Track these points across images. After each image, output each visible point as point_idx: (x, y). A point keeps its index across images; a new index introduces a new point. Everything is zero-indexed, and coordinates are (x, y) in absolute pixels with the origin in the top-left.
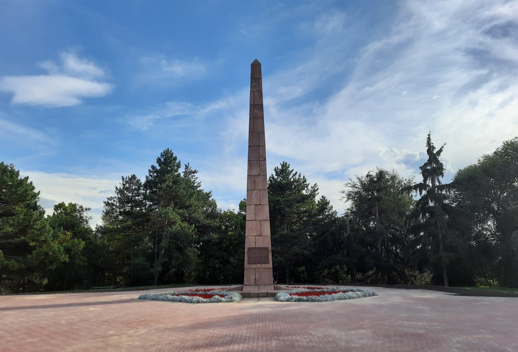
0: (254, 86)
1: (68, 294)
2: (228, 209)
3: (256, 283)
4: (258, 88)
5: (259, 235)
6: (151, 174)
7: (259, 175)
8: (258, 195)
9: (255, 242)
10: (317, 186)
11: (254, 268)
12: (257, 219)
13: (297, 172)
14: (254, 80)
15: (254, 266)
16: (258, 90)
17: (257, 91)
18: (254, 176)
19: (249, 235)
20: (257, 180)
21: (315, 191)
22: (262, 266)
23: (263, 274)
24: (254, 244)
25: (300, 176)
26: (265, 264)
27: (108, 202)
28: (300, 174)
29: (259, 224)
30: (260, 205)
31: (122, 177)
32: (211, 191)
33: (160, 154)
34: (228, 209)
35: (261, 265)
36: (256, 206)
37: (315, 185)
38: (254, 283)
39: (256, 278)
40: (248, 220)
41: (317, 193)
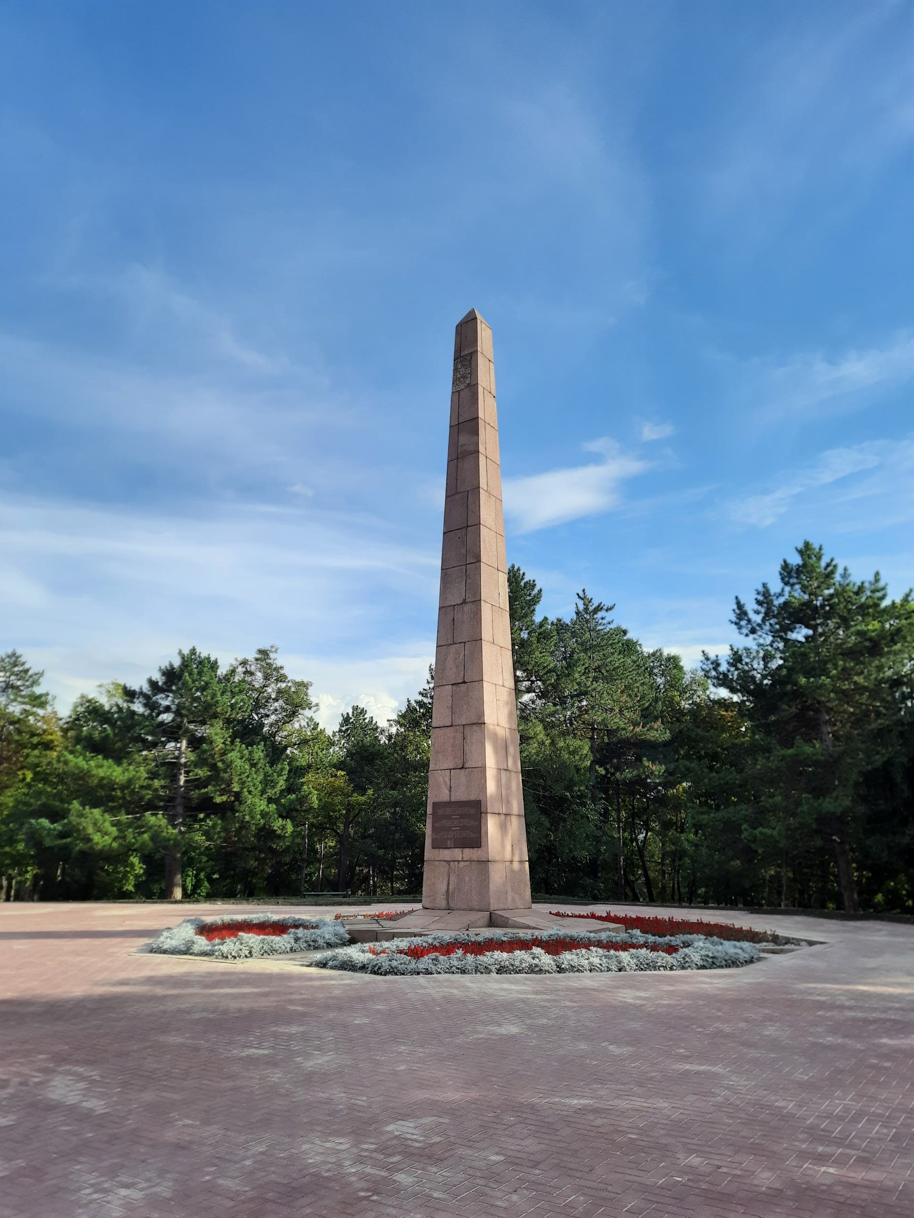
0: (459, 378)
5: (460, 766)
7: (464, 602)
11: (446, 859)
14: (461, 362)
15: (446, 854)
20: (458, 616)
23: (467, 878)
24: (448, 792)
28: (845, 569)
29: (459, 736)
30: (464, 682)
35: (462, 852)
36: (454, 687)
38: (443, 904)
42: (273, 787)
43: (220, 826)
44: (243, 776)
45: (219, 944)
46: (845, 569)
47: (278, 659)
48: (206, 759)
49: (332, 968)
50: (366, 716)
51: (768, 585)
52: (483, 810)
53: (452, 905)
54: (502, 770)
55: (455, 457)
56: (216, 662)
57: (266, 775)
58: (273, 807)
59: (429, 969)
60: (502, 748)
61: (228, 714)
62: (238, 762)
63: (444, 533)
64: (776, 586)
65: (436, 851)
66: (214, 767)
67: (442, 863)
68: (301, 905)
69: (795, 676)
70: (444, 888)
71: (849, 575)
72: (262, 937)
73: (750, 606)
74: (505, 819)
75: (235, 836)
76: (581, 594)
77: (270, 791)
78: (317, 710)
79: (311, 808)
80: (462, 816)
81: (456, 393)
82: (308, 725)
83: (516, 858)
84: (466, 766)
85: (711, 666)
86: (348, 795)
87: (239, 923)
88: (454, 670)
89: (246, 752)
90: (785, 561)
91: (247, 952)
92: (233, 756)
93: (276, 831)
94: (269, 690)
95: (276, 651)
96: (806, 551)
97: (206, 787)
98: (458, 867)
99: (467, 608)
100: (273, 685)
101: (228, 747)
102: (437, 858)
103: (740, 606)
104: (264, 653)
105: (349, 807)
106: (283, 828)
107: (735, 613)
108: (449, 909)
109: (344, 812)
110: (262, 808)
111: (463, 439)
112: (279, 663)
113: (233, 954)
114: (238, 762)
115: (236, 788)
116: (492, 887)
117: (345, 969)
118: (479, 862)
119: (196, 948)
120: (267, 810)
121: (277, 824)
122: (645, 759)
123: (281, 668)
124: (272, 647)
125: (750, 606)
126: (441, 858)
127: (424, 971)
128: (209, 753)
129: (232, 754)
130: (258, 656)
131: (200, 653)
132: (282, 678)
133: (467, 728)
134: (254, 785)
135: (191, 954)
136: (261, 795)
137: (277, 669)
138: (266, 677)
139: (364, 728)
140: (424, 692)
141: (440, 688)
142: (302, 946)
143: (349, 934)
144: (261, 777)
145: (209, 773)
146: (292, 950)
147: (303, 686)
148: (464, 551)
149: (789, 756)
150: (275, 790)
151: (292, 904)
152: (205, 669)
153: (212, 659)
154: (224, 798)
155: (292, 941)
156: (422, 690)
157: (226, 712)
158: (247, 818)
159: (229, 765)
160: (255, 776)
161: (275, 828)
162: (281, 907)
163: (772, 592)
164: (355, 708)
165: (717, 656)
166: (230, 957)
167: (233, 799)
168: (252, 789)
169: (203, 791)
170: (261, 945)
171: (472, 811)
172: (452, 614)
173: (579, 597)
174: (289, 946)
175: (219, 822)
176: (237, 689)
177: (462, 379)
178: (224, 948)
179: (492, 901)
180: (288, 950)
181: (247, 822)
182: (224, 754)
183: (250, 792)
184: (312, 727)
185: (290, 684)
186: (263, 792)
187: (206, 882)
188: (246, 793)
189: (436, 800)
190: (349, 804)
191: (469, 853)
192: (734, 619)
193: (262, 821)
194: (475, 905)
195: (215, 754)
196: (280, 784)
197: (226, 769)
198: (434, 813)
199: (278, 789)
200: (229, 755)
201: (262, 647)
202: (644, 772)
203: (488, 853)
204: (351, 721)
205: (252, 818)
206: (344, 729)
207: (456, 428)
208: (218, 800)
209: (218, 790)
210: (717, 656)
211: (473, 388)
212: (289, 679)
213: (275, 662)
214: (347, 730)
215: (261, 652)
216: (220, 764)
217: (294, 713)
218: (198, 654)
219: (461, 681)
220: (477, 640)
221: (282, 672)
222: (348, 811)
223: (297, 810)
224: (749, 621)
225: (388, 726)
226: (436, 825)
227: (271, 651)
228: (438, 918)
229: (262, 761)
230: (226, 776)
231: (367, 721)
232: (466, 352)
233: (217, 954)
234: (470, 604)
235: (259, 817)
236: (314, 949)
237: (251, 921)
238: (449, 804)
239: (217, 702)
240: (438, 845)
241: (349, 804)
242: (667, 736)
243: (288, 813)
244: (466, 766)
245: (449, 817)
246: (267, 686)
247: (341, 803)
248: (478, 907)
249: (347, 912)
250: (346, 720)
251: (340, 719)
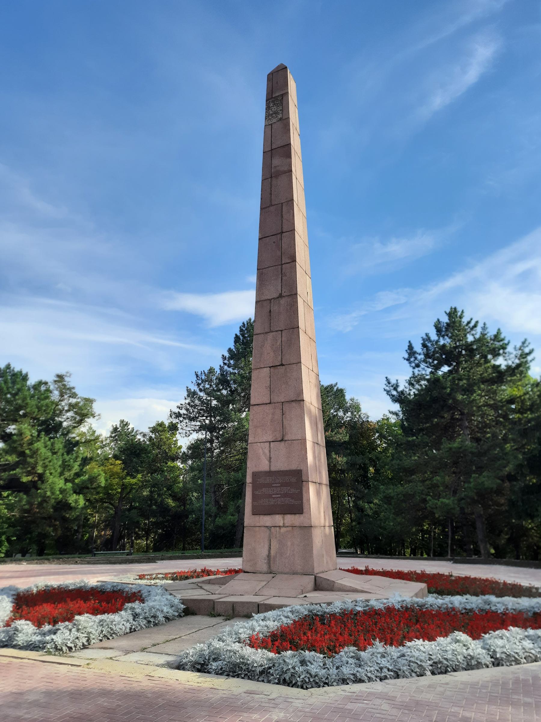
0: (272, 114)
1: (65, 563)
2: (384, 414)
3: (270, 567)
4: (280, 116)
5: (280, 439)
6: (226, 362)
7: (281, 296)
8: (278, 343)
9: (270, 458)
10: (529, 343)
11: (267, 525)
12: (276, 399)
13: (477, 322)
14: (273, 102)
15: (267, 520)
16: (281, 119)
17: (278, 121)
18: (269, 301)
19: (256, 440)
20: (275, 308)
21: (524, 356)
22: (286, 521)
23: (289, 544)
24: (267, 462)
25: (484, 328)
26: (293, 516)
27: (179, 412)
28: (485, 324)
29: (278, 412)
30: (282, 365)
31: (196, 372)
32: (337, 383)
33: (239, 329)
34: (384, 414)
35: (283, 518)
36: (272, 369)
37: (524, 343)
38: (265, 568)
39: (273, 553)
40: (254, 403)
41: (529, 358)
42: (70, 470)
43: (25, 500)
44: (46, 461)
45: (50, 632)
46: (485, 324)
47: (71, 382)
48: (16, 448)
49: (220, 673)
50: (129, 427)
51: (429, 335)
52: (304, 478)
53: (274, 569)
54: (316, 443)
55: (269, 176)
56: (26, 375)
57: (64, 461)
58: (69, 485)
59: (358, 674)
60: (314, 425)
61: (36, 414)
62: (43, 450)
63: (260, 239)
64: (434, 337)
65: (257, 517)
66: (22, 454)
67: (262, 528)
68: (97, 564)
69: (454, 394)
70: (265, 552)
71: (487, 328)
72: (99, 617)
73: (418, 348)
74: (319, 487)
75: (37, 508)
77: (66, 473)
78: (99, 418)
79: (99, 486)
80: (283, 485)
81: (269, 127)
82: (88, 432)
83: (327, 524)
84: (286, 438)
85: (392, 388)
86: (122, 478)
87: (54, 589)
88: (272, 354)
89: (49, 443)
90: (438, 320)
91: (84, 640)
92: (38, 445)
93: (71, 504)
94: (63, 403)
95: (70, 376)
96: (453, 314)
97: (14, 469)
98: (280, 532)
99: (283, 301)
100: (66, 401)
101: (35, 439)
102: (258, 524)
103: (410, 347)
105: (124, 487)
106: (76, 501)
107: (408, 353)
108: (271, 573)
109: (119, 490)
110: (60, 486)
111: (277, 162)
112: (71, 385)
113: (69, 645)
114: (43, 450)
115: (40, 470)
116: (315, 552)
117: (238, 676)
118: (301, 527)
119: (21, 639)
120: (64, 487)
121: (72, 498)
122: (333, 453)
123: (73, 388)
124: (67, 373)
125: (418, 348)
126: (262, 523)
127: (352, 677)
128: (18, 443)
129: (38, 443)
131: (14, 368)
132: (74, 395)
133: (286, 406)
134: (54, 468)
135: (14, 647)
136: (60, 476)
137: (70, 389)
138: (62, 395)
139: (128, 434)
140: (181, 406)
141: (258, 371)
142: (142, 624)
143: (183, 603)
144: (60, 463)
145: (17, 460)
146: (132, 631)
147: (89, 401)
148: (279, 253)
149: (455, 448)
150: (71, 472)
151: (89, 563)
152: (18, 380)
153: (24, 372)
154: (30, 478)
155: (131, 618)
156: (179, 405)
157: (34, 412)
158: (49, 493)
159: (35, 453)
160: (55, 461)
161: (70, 502)
162: (80, 566)
164: (122, 421)
165: (397, 381)
166: (64, 648)
167: (36, 479)
168: (53, 471)
169: (12, 472)
170: (100, 628)
171: (294, 480)
172: (269, 307)
174: (128, 625)
175: (25, 497)
176: (43, 396)
177: (274, 115)
178: (58, 638)
179: (316, 565)
180: (128, 631)
181: (48, 497)
182: (31, 443)
183: (51, 474)
184: (91, 433)
185: (79, 400)
186: (61, 474)
187: (6, 543)
188: (49, 474)
189: (256, 470)
190: (123, 485)
191: (290, 519)
192: (406, 356)
193: (61, 496)
194: (299, 568)
195: (24, 443)
196: (75, 468)
197: (33, 455)
198: (254, 482)
199: (73, 472)
200: (35, 445)
201: (60, 373)
202: (332, 462)
203: (310, 519)
204: (118, 430)
205: (53, 493)
206: (113, 435)
207: (269, 153)
208: (25, 479)
209: (24, 472)
210: (397, 381)
211: (285, 122)
212: (79, 396)
213: (69, 383)
214: (116, 436)
216: (27, 452)
217: (82, 420)
218: (12, 368)
219: (278, 364)
220: (294, 328)
221: (73, 391)
222: (123, 489)
223: (88, 488)
225: (149, 431)
226: (257, 493)
227: (66, 376)
228: (264, 583)
229: (61, 450)
230: (32, 460)
231: (129, 430)
232: (277, 95)
233: (49, 646)
234: (286, 298)
235: (58, 492)
236: (154, 625)
237: (67, 586)
238: (270, 473)
239: (27, 404)
240: (255, 512)
241: (123, 485)
242: (347, 438)
243: (80, 490)
244: (286, 438)
245: (269, 486)
246: (62, 401)
247: (117, 484)
248: (302, 571)
249: (144, 570)
250: (115, 430)
251: (111, 429)
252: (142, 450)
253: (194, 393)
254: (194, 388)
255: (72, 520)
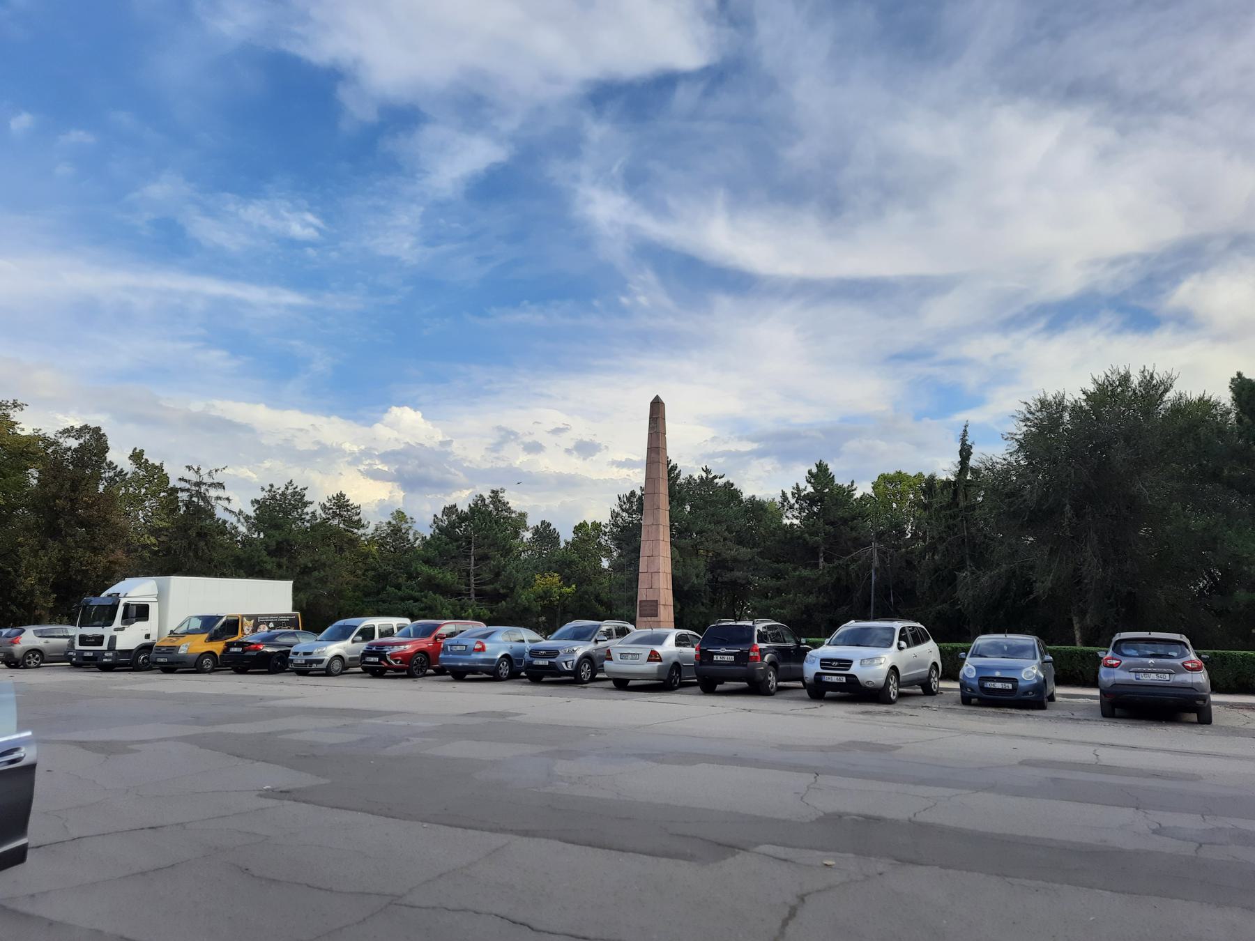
7: (653, 524)
15: (645, 619)
20: (650, 530)
76: (705, 468)
86: (560, 588)
99: (654, 527)
104: (495, 493)
105: (561, 595)
130: (492, 495)
154: (505, 591)
163: (801, 488)
164: (543, 522)
171: (655, 604)
173: (703, 470)
190: (561, 593)
191: (653, 618)
198: (1089, 653)
215: (493, 492)
224: (789, 502)
240: (640, 616)
241: (561, 593)
245: (645, 606)
252: (572, 561)
253: (618, 514)
254: (617, 510)
255: (1211, 550)
